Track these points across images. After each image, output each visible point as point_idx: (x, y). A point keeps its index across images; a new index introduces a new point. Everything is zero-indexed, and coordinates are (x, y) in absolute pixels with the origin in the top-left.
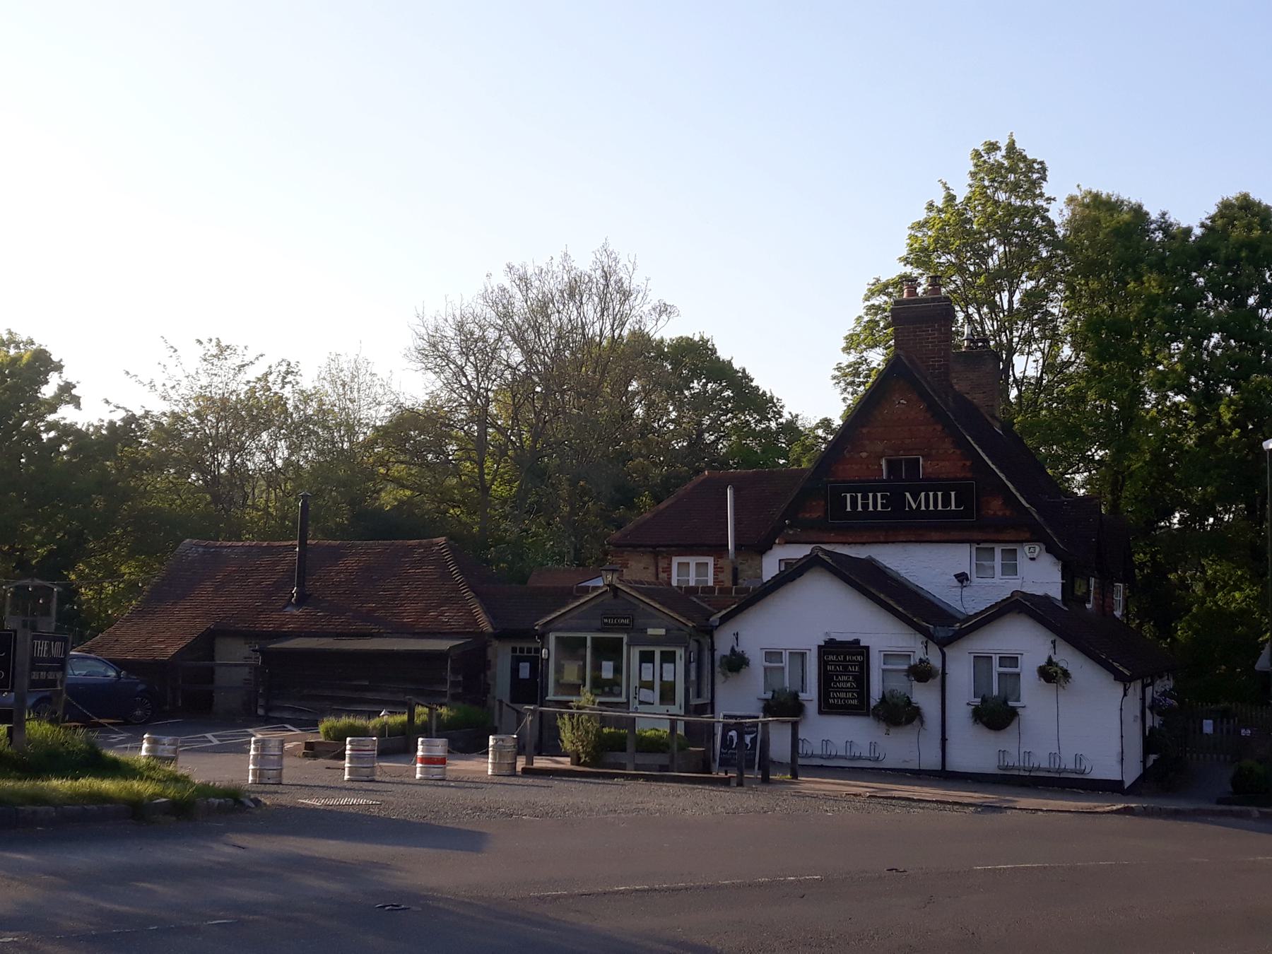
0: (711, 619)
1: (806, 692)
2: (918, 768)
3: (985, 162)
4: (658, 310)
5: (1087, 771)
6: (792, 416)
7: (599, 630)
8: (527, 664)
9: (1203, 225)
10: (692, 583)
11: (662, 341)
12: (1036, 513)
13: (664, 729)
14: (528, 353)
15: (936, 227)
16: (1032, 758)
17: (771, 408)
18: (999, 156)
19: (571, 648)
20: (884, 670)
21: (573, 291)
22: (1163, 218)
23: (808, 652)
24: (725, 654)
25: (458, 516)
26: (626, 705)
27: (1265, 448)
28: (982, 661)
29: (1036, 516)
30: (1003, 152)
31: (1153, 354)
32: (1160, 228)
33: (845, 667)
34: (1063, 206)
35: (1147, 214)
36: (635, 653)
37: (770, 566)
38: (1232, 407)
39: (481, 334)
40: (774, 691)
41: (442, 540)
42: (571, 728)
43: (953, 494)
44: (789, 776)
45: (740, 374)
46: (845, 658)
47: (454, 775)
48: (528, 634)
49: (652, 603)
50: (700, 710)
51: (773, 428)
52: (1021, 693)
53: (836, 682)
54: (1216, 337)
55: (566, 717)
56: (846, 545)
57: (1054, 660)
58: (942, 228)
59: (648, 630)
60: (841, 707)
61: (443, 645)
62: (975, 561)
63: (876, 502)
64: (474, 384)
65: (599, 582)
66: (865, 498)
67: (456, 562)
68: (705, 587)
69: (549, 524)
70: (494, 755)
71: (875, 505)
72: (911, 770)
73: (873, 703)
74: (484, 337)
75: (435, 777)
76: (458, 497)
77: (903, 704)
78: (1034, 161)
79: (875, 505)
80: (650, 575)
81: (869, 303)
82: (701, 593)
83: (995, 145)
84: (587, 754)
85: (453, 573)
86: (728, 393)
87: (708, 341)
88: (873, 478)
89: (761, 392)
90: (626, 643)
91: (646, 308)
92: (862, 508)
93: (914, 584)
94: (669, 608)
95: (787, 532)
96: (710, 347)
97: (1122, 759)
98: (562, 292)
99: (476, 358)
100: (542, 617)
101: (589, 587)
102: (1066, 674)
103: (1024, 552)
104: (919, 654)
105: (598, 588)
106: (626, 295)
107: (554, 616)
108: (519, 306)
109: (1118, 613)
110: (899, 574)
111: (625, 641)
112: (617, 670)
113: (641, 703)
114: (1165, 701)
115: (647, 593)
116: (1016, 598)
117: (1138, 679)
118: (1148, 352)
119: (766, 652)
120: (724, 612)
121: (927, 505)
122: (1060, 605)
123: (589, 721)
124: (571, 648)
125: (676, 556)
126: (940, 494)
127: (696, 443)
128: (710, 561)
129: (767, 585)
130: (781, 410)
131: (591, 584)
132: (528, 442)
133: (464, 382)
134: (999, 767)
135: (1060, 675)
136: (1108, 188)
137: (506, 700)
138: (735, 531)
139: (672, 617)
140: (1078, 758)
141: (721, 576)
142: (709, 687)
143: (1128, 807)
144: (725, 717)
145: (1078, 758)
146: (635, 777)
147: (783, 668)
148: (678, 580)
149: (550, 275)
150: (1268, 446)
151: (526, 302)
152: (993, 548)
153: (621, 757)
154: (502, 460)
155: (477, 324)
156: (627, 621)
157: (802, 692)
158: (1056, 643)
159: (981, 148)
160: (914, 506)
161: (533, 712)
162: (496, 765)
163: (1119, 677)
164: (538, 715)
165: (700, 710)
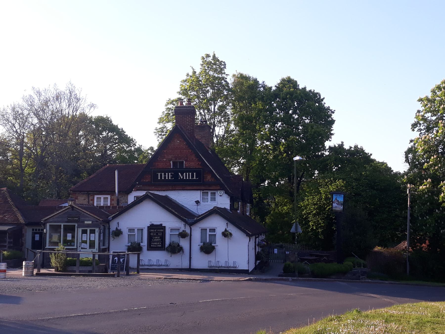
3: (205, 61)
4: (90, 106)
5: (237, 267)
8: (38, 235)
9: (276, 86)
10: (102, 205)
11: (92, 117)
12: (222, 180)
13: (91, 257)
14: (40, 120)
17: (132, 142)
18: (210, 59)
19: (55, 229)
20: (170, 234)
21: (58, 98)
27: (294, 160)
28: (204, 231)
29: (222, 181)
30: (212, 58)
31: (260, 128)
32: (262, 87)
33: (157, 234)
34: (231, 78)
36: (80, 230)
37: (131, 199)
40: (131, 243)
41: (5, 189)
42: (55, 258)
43: (195, 173)
44: (136, 273)
45: (121, 130)
46: (157, 230)
47: (9, 276)
48: (38, 224)
49: (87, 212)
50: (104, 250)
53: (154, 239)
54: (280, 124)
55: (53, 254)
57: (227, 230)
59: (85, 222)
60: (155, 248)
61: (6, 228)
63: (169, 176)
64: (19, 131)
65: (66, 205)
66: (165, 175)
67: (11, 197)
68: (107, 206)
70: (25, 269)
71: (168, 177)
73: (166, 246)
75: (2, 277)
78: (222, 61)
79: (168, 177)
86: (116, 137)
87: (109, 118)
88: (168, 168)
89: (128, 137)
91: (86, 105)
92: (164, 178)
93: (181, 204)
94: (93, 214)
96: (110, 120)
97: (248, 262)
98: (53, 98)
100: (44, 218)
101: (62, 206)
102: (231, 234)
103: (218, 193)
104: (183, 228)
105: (65, 207)
106: (78, 100)
107: (48, 217)
109: (248, 214)
111: (76, 226)
112: (73, 237)
113: (82, 248)
115: (84, 208)
118: (258, 128)
121: (186, 177)
122: (230, 211)
123: (61, 255)
124: (55, 229)
126: (190, 173)
128: (109, 197)
131: (63, 205)
133: (15, 130)
134: (208, 267)
136: (246, 72)
137: (30, 248)
140: (234, 263)
141: (113, 202)
143: (250, 278)
144: (113, 252)
145: (234, 263)
146: (79, 275)
147: (135, 234)
149: (49, 91)
152: (208, 192)
153: (75, 268)
157: (142, 243)
159: (204, 56)
160: (182, 178)
161: (40, 252)
163: (248, 235)
165: (104, 250)
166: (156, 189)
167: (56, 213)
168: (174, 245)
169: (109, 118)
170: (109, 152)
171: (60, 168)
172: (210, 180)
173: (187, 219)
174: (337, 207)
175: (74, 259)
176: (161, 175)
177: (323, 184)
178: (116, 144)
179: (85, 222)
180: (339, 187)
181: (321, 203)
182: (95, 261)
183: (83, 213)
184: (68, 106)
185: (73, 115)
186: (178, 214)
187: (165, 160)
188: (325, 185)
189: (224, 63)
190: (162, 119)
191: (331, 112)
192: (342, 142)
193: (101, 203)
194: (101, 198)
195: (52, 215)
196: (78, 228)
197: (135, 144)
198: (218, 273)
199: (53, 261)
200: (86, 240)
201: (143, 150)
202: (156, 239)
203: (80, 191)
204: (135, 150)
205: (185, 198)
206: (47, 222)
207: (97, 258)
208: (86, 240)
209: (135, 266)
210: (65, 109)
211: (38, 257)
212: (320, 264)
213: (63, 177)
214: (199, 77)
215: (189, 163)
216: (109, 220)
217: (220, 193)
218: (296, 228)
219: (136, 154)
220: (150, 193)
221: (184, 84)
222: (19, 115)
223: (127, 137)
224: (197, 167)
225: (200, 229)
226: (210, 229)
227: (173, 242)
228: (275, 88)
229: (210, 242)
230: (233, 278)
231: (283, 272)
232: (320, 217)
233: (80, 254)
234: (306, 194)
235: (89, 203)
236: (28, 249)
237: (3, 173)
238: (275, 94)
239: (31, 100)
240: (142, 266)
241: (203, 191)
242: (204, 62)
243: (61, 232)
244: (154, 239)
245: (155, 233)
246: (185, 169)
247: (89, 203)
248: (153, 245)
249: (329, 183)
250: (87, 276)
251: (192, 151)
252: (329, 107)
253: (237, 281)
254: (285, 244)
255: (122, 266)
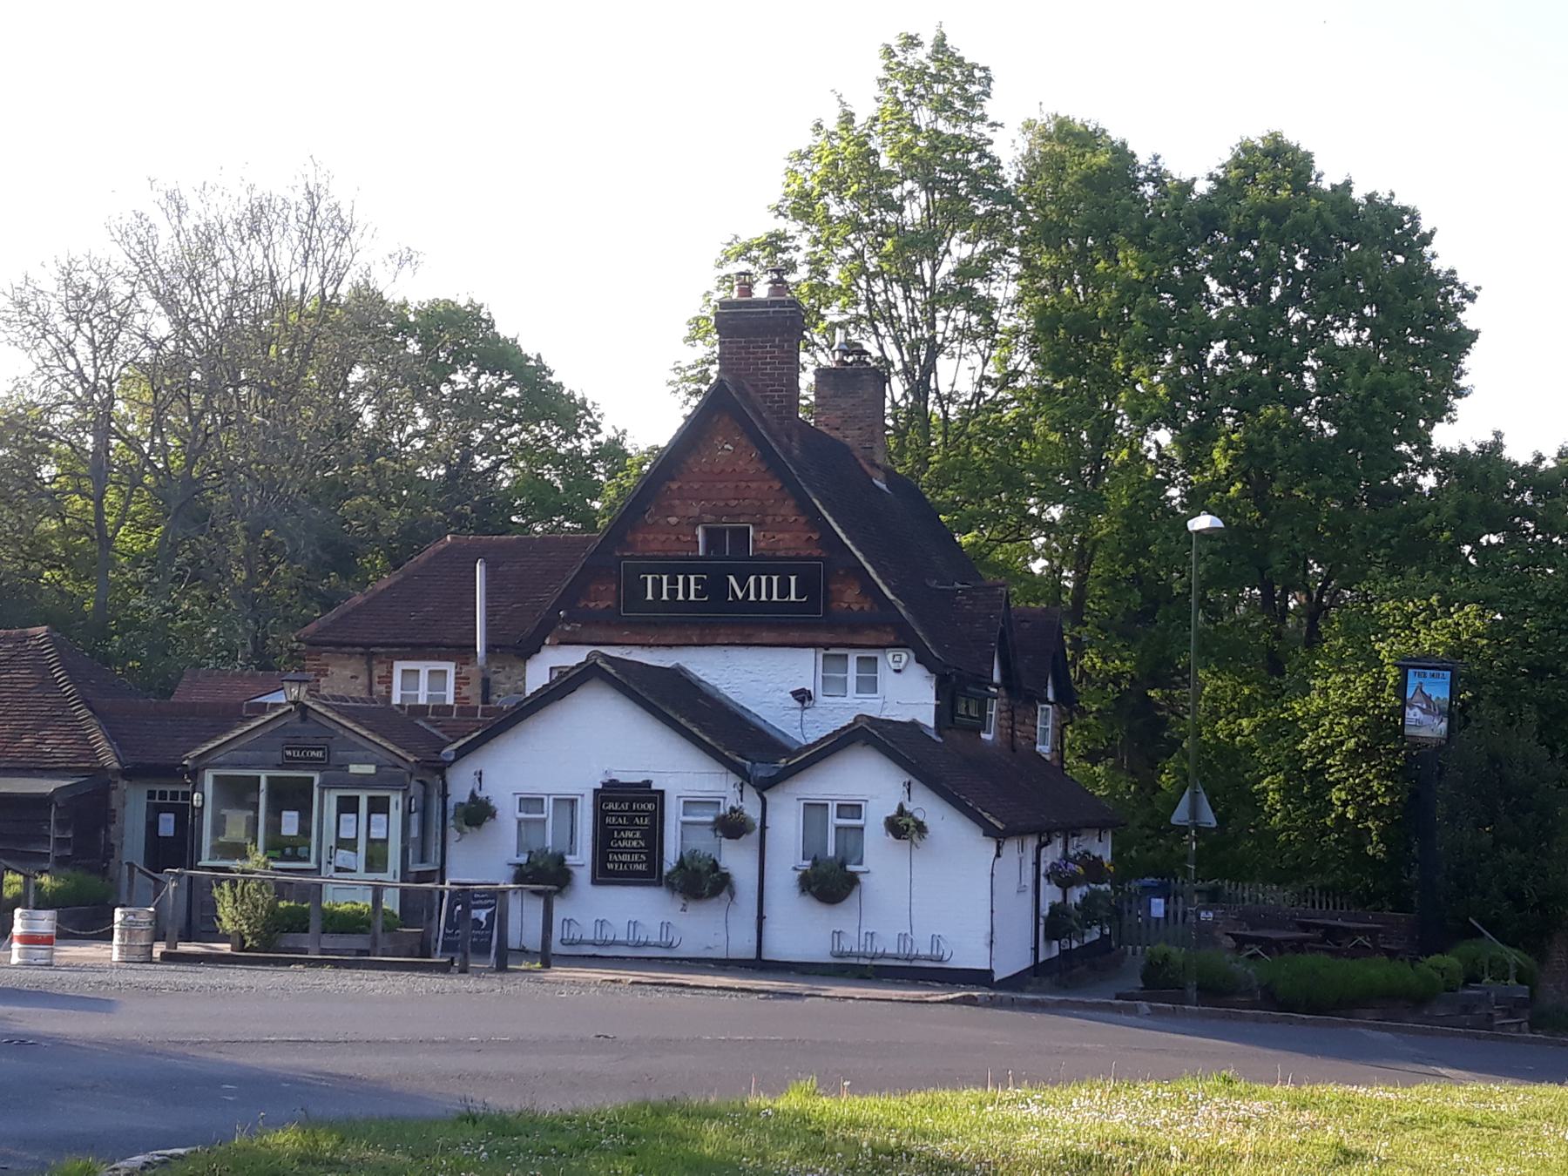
0: (443, 752)
1: (575, 854)
2: (725, 957)
3: (899, 64)
4: (397, 257)
5: (946, 957)
6: (616, 431)
7: (279, 767)
8: (172, 816)
9: (1211, 177)
10: (422, 701)
11: (404, 305)
12: (904, 608)
15: (823, 161)
16: (875, 943)
17: (582, 417)
18: (920, 55)
19: (237, 792)
20: (684, 823)
21: (256, 222)
22: (1156, 163)
23: (579, 798)
24: (462, 801)
25: (58, 582)
26: (318, 871)
27: (1190, 529)
28: (814, 810)
29: (904, 612)
30: (928, 48)
31: (1128, 369)
32: (1149, 178)
33: (631, 820)
34: (1017, 135)
35: (1133, 155)
36: (331, 798)
37: (537, 674)
38: (1230, 451)
39: (102, 286)
40: (530, 853)
41: (41, 630)
42: (232, 901)
43: (793, 578)
44: (538, 965)
45: (532, 363)
46: (631, 806)
47: (64, 961)
48: (172, 771)
49: (356, 729)
50: (422, 877)
51: (586, 449)
52: (865, 856)
53: (618, 840)
54: (1218, 348)
55: (226, 885)
56: (646, 648)
57: (907, 809)
58: (834, 164)
59: (351, 766)
61: (46, 786)
62: (855, 674)
63: (689, 588)
64: (89, 372)
65: (279, 698)
67: (64, 665)
68: (440, 706)
69: (211, 599)
70: (122, 934)
72: (717, 959)
73: (667, 868)
74: (107, 290)
75: (39, 961)
76: (57, 550)
77: (706, 868)
78: (974, 66)
80: (360, 688)
81: (723, 272)
82: (432, 714)
83: (915, 38)
84: (255, 936)
85: (60, 680)
86: (513, 392)
87: (481, 307)
88: (685, 554)
89: (565, 392)
90: (318, 786)
92: (668, 595)
93: (737, 704)
94: (381, 736)
95: (563, 629)
96: (485, 317)
97: (992, 941)
99: (92, 327)
100: (194, 748)
101: (266, 704)
102: (921, 828)
103: (888, 660)
104: (732, 800)
105: (276, 706)
106: (345, 232)
107: (211, 745)
108: (167, 247)
109: (1044, 749)
110: (717, 690)
111: (316, 782)
113: (338, 869)
114: (1066, 865)
116: (860, 724)
117: (1032, 833)
118: (1121, 366)
119: (521, 799)
120: (462, 742)
121: (758, 594)
122: (933, 736)
123: (258, 890)
125: (400, 660)
126: (775, 578)
127: (459, 472)
128: (450, 667)
129: (525, 704)
130: (599, 420)
131: (269, 699)
132: (178, 463)
133: (72, 365)
134: (833, 954)
135: (912, 829)
136: (1083, 114)
137: (140, 864)
138: (487, 625)
139: (385, 748)
140: (936, 940)
141: (465, 691)
142: (439, 847)
143: (969, 996)
144: (452, 884)
145: (936, 940)
146: (319, 963)
147: (544, 821)
148: (402, 695)
149: (218, 191)
150: (1193, 525)
151: (178, 235)
152: (846, 656)
153: (305, 940)
154: (135, 493)
155: (95, 272)
156: (319, 754)
157: (570, 854)
158: (912, 785)
160: (740, 595)
162: (125, 949)
163: (989, 831)
164: (185, 880)
165: (422, 877)
166: (638, 639)
167: (239, 732)
168: (696, 864)
169: (481, 307)
170: (481, 463)
171: (268, 533)
172: (856, 607)
173: (748, 763)
174: (1424, 724)
175: (305, 906)
176: (658, 584)
177: (1394, 621)
178: (514, 422)
179: (351, 766)
180: (1465, 637)
181: (1379, 707)
182: (380, 915)
183: (341, 732)
184: (300, 260)
185: (323, 298)
186: (713, 744)
187: (673, 520)
188: (1403, 628)
189: (983, 74)
190: (702, 323)
191: (1463, 297)
192: (1498, 434)
193: (427, 693)
194: (418, 671)
195: (225, 739)
196: (324, 788)
197: (595, 426)
198: (869, 978)
199: (228, 914)
200: (353, 836)
201: (630, 451)
202: (628, 839)
203: (340, 643)
204: (594, 451)
205: (752, 677)
206: (208, 766)
207: (391, 902)
208: (353, 836)
209: (533, 940)
210: (291, 273)
211: (171, 891)
212: (1307, 960)
213: (278, 574)
214: (869, 135)
215: (769, 535)
216: (445, 762)
217: (897, 659)
218: (1194, 811)
219: (602, 471)
220: (603, 655)
221: (801, 169)
222: (93, 301)
223: (561, 394)
224: (803, 553)
225: (802, 802)
226: (839, 806)
227: (693, 854)
228: (1211, 184)
229: (839, 859)
230: (902, 992)
231: (1141, 985)
232: (1375, 766)
233: (324, 885)
234: (1318, 666)
235: (371, 692)
236: (134, 866)
237: (22, 551)
238: (1202, 216)
239: (141, 231)
240: (570, 944)
241: (827, 649)
242: (892, 69)
243: (257, 805)
244: (618, 840)
245: (622, 817)
246: (751, 558)
247: (371, 692)
248: (614, 862)
249: (1421, 618)
250: (349, 965)
251: (781, 488)
252: (1453, 272)
253: (913, 1002)
254: (1230, 886)
255: (484, 936)
